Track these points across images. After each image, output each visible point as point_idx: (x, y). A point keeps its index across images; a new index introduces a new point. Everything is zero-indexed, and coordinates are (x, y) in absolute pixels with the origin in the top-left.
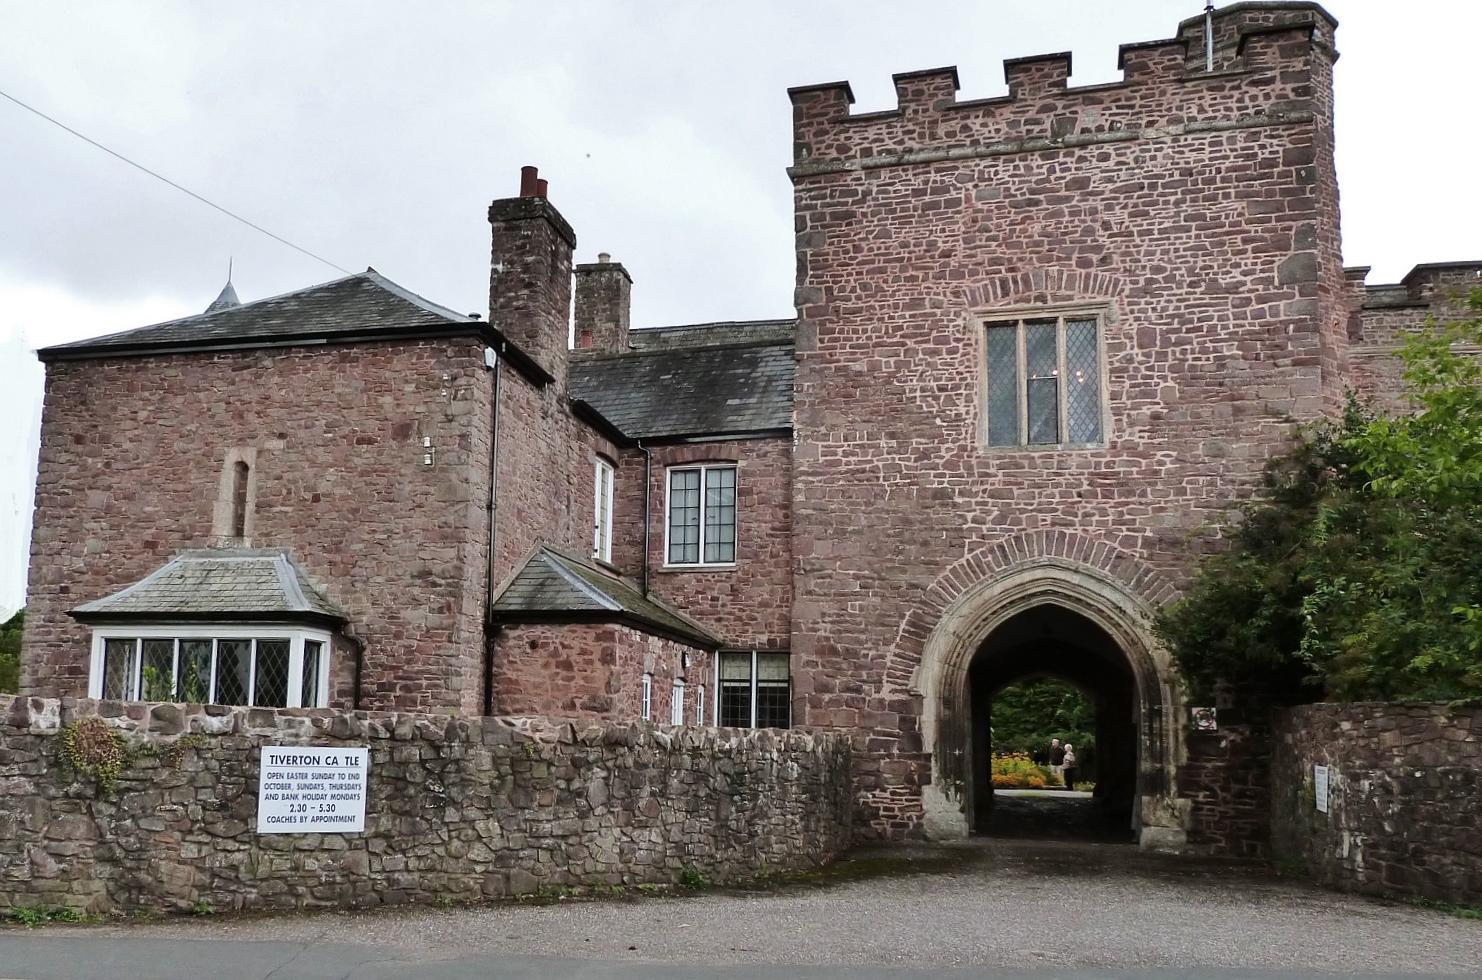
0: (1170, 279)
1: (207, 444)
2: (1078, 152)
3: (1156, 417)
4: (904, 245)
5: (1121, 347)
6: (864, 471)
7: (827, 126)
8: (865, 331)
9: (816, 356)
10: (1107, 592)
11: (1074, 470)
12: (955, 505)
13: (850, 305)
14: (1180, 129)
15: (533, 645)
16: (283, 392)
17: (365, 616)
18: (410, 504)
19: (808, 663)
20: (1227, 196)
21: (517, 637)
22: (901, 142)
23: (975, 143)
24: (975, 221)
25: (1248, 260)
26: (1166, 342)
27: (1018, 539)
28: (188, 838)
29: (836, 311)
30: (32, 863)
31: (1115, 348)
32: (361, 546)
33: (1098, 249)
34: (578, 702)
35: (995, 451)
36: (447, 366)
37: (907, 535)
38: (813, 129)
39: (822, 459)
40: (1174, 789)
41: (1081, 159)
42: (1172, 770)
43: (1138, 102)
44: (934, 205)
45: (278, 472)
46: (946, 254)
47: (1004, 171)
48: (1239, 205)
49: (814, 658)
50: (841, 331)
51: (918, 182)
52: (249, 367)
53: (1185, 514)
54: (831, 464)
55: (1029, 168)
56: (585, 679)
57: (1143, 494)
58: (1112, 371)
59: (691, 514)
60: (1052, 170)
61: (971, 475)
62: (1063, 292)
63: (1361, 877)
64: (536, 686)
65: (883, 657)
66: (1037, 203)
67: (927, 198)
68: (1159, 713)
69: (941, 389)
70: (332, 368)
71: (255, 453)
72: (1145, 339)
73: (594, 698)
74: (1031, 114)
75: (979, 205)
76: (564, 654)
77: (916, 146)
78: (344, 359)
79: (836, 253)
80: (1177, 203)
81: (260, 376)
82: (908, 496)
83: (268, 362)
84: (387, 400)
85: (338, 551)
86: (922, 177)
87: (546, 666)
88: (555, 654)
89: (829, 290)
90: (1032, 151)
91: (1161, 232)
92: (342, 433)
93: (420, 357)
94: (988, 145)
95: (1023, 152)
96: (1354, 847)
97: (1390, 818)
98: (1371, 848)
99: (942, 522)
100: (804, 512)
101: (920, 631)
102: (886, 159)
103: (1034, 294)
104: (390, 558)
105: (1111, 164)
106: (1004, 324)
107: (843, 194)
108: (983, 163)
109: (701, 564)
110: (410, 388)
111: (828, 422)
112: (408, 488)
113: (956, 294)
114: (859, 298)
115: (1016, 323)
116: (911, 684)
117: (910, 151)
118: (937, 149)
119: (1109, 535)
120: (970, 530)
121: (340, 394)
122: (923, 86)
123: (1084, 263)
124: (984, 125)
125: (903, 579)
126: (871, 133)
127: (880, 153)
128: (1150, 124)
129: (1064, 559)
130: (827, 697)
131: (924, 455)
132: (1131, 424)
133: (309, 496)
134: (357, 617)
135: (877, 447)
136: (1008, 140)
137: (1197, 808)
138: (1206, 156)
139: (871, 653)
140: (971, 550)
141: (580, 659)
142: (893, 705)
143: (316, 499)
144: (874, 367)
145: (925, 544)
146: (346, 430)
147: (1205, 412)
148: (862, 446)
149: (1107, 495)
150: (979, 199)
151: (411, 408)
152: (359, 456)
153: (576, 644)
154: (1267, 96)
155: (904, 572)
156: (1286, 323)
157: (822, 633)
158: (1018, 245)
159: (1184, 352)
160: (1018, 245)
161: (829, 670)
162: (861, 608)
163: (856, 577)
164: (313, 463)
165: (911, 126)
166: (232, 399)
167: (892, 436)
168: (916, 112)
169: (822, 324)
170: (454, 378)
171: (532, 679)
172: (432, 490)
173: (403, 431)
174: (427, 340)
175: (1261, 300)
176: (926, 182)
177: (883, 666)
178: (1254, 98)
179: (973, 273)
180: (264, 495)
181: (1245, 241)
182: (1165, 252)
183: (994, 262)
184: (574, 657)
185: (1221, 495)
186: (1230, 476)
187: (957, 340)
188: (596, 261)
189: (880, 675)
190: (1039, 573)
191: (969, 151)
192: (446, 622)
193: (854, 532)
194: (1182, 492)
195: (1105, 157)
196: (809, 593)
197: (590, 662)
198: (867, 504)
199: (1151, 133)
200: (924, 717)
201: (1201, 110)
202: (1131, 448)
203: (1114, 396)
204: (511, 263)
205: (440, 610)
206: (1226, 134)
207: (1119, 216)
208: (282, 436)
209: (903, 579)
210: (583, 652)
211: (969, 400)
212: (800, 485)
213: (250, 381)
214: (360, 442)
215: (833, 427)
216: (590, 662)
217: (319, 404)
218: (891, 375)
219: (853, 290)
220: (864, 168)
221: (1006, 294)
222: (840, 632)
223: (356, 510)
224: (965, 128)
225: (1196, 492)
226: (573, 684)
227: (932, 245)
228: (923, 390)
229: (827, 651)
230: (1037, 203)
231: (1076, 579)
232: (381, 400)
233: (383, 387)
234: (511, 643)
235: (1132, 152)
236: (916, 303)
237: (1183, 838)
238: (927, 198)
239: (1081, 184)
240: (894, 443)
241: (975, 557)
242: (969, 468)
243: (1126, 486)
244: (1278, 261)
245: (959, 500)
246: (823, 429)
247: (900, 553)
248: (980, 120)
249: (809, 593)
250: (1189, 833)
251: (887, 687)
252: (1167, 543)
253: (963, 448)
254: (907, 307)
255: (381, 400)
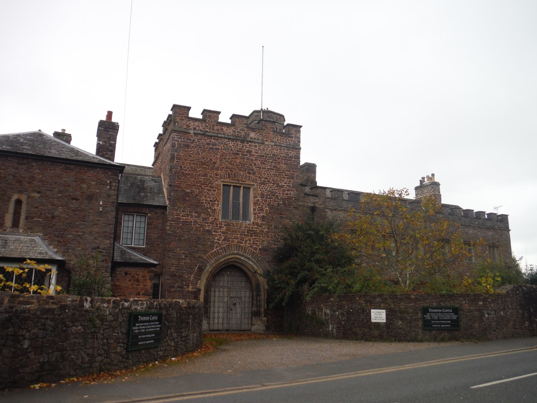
0: (269, 181)
1: (4, 191)
2: (250, 144)
3: (263, 216)
4: (203, 158)
5: (256, 197)
6: (187, 222)
7: (184, 118)
8: (190, 181)
9: (176, 185)
10: (250, 262)
11: (244, 228)
12: (213, 235)
13: (187, 172)
14: (273, 144)
15: (126, 274)
16: (40, 176)
17: (73, 261)
18: (92, 224)
19: (168, 279)
20: (282, 163)
21: (121, 271)
22: (204, 128)
23: (224, 134)
24: (223, 155)
25: (286, 180)
26: (267, 198)
27: (228, 245)
28: (119, 345)
29: (183, 173)
30: (82, 358)
31: (255, 197)
32: (72, 236)
33: (253, 170)
34: (141, 293)
35: (224, 220)
36: (109, 178)
37: (199, 242)
38: (180, 118)
39: (175, 217)
40: (263, 315)
41: (250, 145)
42: (263, 310)
43: (264, 134)
44: (212, 149)
45: (36, 205)
46: (215, 163)
47: (231, 144)
48: (285, 166)
49: (169, 277)
50: (184, 179)
51: (208, 141)
52: (25, 164)
53: (269, 243)
54: (178, 218)
55: (237, 144)
56: (144, 285)
57: (260, 237)
58: (254, 203)
59: (130, 229)
60: (243, 146)
61: (217, 226)
62: (244, 180)
63: (335, 335)
64: (126, 287)
65: (190, 278)
66: (239, 154)
67: (210, 146)
68: (260, 295)
69: (211, 201)
70: (62, 171)
71: (26, 197)
72: (262, 196)
73: (146, 291)
74: (239, 130)
75: (224, 151)
76: (137, 277)
77: (208, 131)
78: (67, 168)
79: (184, 156)
80: (271, 162)
81: (30, 168)
82: (200, 231)
83: (34, 164)
84: (84, 186)
85: (62, 237)
86: (209, 140)
87: (130, 281)
88: (133, 277)
89: (181, 166)
90: (239, 140)
91: (268, 169)
92: (65, 195)
93: (98, 173)
94: (228, 136)
95: (236, 140)
96: (333, 328)
97: (344, 321)
98: (338, 328)
99: (209, 239)
100: (169, 232)
101: (201, 270)
102: (199, 132)
103: (236, 179)
104: (84, 241)
105: (257, 148)
106: (228, 185)
107: (187, 139)
108: (226, 140)
109: (133, 246)
110: (93, 183)
111: (178, 205)
112: (91, 217)
113: (216, 175)
114: (189, 170)
115: (231, 185)
116: (198, 286)
117: (207, 132)
118: (214, 133)
119: (251, 247)
120: (216, 242)
121: (65, 181)
122: (211, 114)
123: (249, 173)
124: (227, 130)
125: (197, 255)
126: (196, 123)
127: (198, 130)
128: (267, 141)
129: (241, 253)
130: (173, 289)
131: (204, 219)
132: (258, 218)
133: (50, 216)
134: (69, 262)
135: (192, 215)
136: (232, 135)
137: (268, 320)
138: (278, 152)
139: (187, 277)
140: (216, 248)
141: (142, 279)
142: (192, 292)
143: (53, 217)
144: (192, 192)
145: (204, 245)
146: (67, 194)
147: (274, 217)
148: (187, 215)
149: (251, 236)
150: (224, 149)
151: (94, 190)
152: (72, 204)
153: (141, 274)
154: (292, 141)
155: (197, 253)
156: (293, 197)
157: (172, 270)
158: (233, 165)
159: (271, 201)
160: (233, 165)
161: (174, 281)
162: (185, 263)
163: (184, 254)
164: (53, 204)
165: (207, 125)
166: (16, 175)
167: (196, 212)
168: (209, 121)
169: (178, 176)
170: (111, 183)
171: (125, 285)
172: (101, 219)
173: (90, 198)
174: (101, 168)
175: (288, 191)
176: (210, 141)
177: (190, 280)
178: (289, 140)
179: (221, 170)
180: (30, 213)
181: (285, 175)
182: (268, 174)
183: (227, 168)
184: (140, 278)
185: (277, 239)
186: (279, 234)
187: (216, 188)
188: (60, 131)
189: (189, 283)
190: (233, 256)
191: (223, 136)
192: (105, 265)
193: (183, 240)
194: (268, 237)
195: (256, 147)
196: (169, 257)
197: (146, 280)
198: (188, 232)
199: (267, 143)
200: (201, 296)
201: (278, 140)
202: (257, 224)
203: (254, 210)
204: (105, 142)
205: (103, 261)
206: (283, 148)
207: (258, 163)
208: (39, 192)
209: (197, 255)
210: (143, 277)
211: (218, 205)
212: (168, 224)
213: (25, 170)
214: (73, 199)
215: (179, 207)
216: (146, 280)
217: (56, 183)
218: (197, 195)
219: (188, 168)
220: (194, 133)
221: (229, 177)
222: (177, 270)
223: (70, 223)
224: (222, 129)
225: (272, 237)
226: (139, 287)
227: (211, 160)
228: (206, 200)
229: (173, 275)
230: (239, 154)
231: (243, 258)
232: (82, 185)
233: (83, 181)
234: (118, 272)
235: (262, 147)
236: (205, 175)
237: (264, 328)
238: (210, 146)
239: (250, 152)
240: (196, 215)
241: (217, 250)
242: (217, 224)
243: (255, 234)
244: (292, 181)
245: (214, 233)
246: (176, 208)
247: (197, 247)
248: (226, 128)
249: (169, 257)
250: (266, 327)
251: (191, 287)
252: (264, 250)
253: (215, 219)
254: (203, 176)
255: (82, 185)
